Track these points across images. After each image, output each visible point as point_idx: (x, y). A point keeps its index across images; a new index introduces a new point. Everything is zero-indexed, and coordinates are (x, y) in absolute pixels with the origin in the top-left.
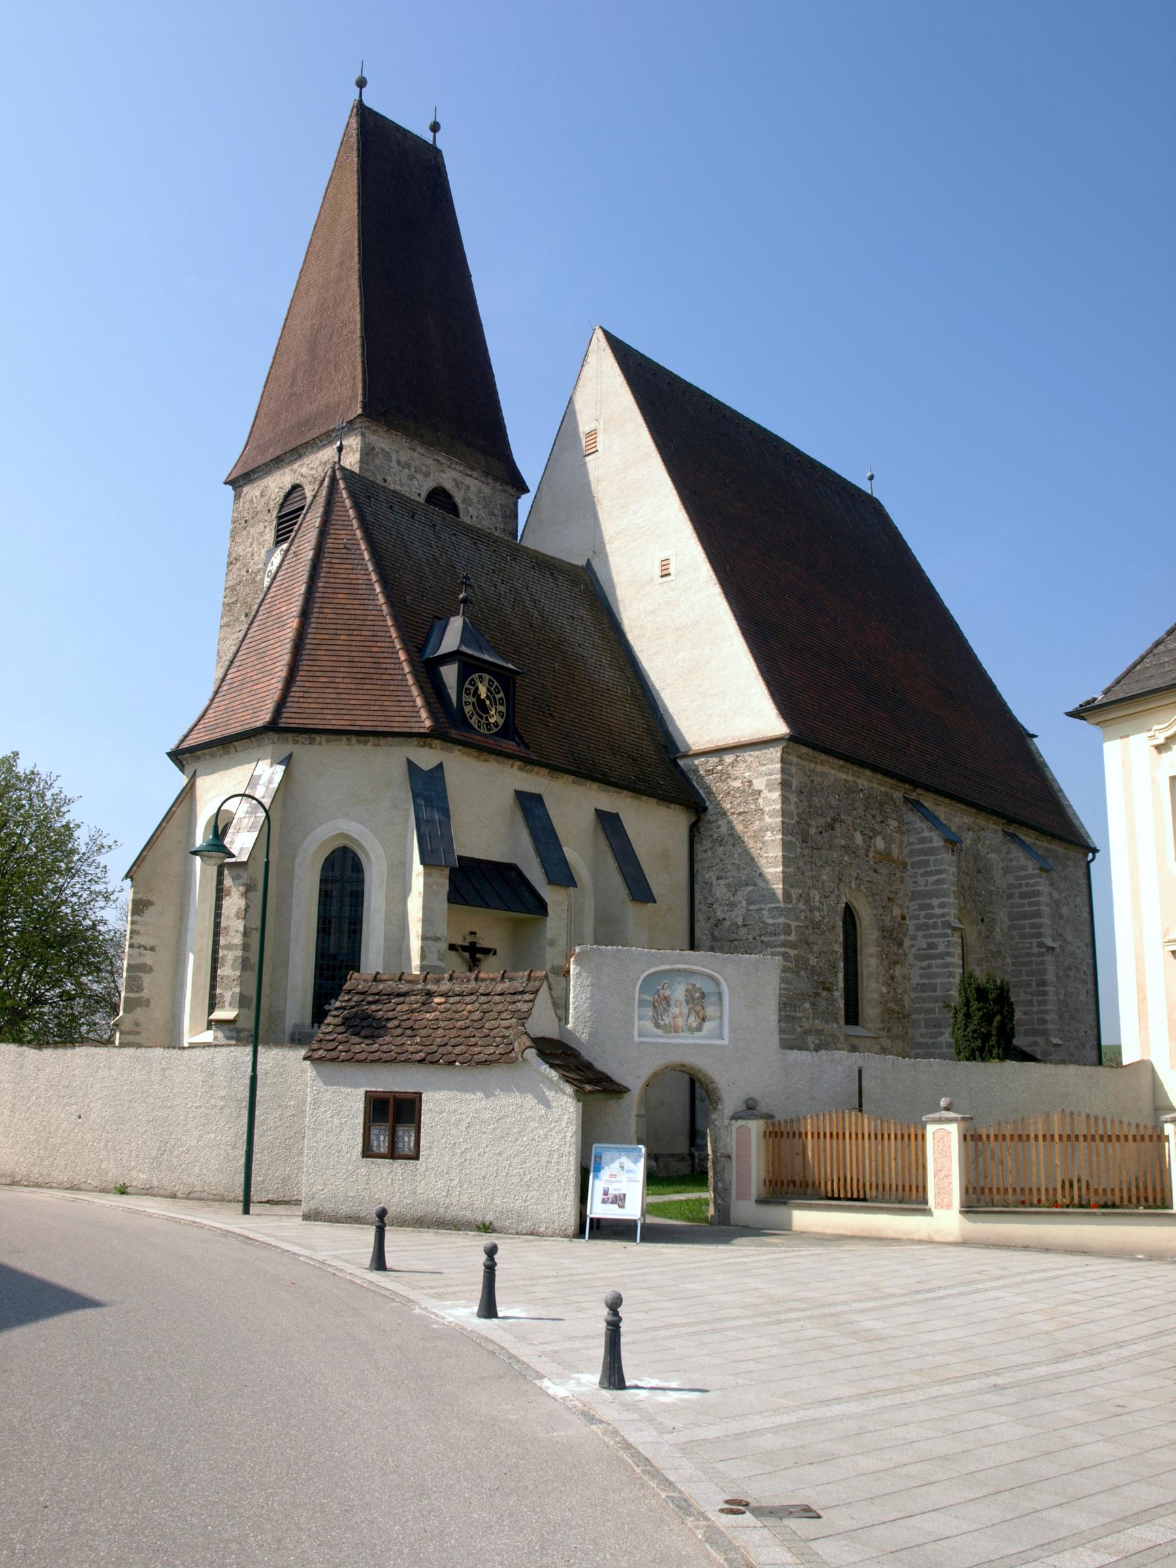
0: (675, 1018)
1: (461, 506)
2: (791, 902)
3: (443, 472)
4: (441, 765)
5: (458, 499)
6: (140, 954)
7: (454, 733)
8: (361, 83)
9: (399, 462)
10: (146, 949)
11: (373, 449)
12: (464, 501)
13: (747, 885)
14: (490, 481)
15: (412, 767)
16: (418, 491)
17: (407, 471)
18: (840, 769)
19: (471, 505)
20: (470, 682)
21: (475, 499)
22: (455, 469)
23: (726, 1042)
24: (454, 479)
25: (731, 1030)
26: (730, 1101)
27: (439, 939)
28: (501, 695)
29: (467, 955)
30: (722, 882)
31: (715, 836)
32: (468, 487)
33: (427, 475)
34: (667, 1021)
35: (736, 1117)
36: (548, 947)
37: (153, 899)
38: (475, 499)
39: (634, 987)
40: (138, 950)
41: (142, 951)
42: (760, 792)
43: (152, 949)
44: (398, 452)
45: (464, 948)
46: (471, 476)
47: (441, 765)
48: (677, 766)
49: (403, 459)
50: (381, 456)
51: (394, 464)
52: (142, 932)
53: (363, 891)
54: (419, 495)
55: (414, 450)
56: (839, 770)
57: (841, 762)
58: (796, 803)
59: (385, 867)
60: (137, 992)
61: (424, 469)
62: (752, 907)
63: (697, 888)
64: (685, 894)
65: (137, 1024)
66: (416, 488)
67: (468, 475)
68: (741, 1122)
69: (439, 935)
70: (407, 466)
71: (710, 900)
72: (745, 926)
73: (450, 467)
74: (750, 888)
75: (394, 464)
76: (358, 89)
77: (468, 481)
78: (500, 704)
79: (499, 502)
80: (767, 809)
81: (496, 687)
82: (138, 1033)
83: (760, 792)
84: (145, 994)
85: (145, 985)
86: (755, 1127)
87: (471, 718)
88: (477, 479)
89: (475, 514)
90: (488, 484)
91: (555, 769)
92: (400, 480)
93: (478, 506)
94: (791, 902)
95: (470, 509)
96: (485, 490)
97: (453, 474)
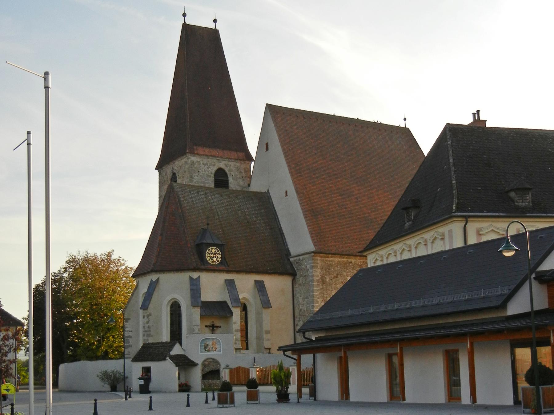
0: (209, 348)
1: (228, 173)
2: (318, 303)
3: (220, 162)
4: (199, 277)
5: (227, 171)
6: (128, 333)
7: (203, 267)
8: (184, 15)
9: (203, 164)
10: (130, 331)
11: (193, 162)
12: (229, 170)
13: (307, 298)
14: (239, 161)
15: (191, 278)
16: (211, 172)
17: (207, 166)
18: (340, 258)
19: (232, 171)
20: (208, 250)
21: (233, 169)
22: (225, 161)
23: (221, 353)
24: (225, 164)
25: (222, 350)
26: (223, 366)
27: (198, 325)
28: (220, 252)
29: (211, 328)
30: (301, 297)
31: (299, 283)
32: (231, 165)
33: (214, 165)
34: (208, 349)
35: (224, 369)
36: (234, 325)
37: (130, 318)
38: (233, 169)
39: (199, 342)
40: (128, 332)
41: (129, 332)
42: (309, 269)
43: (131, 331)
44: (202, 160)
45: (210, 326)
46: (231, 161)
47: (199, 277)
48: (290, 260)
49: (205, 162)
50: (196, 163)
51: (202, 165)
52: (128, 327)
53: (181, 313)
54: (212, 173)
55: (209, 158)
56: (339, 258)
57: (339, 256)
58: (320, 272)
59: (186, 306)
60: (128, 343)
61: (213, 164)
62: (308, 305)
63: (295, 300)
64: (291, 301)
65: (129, 352)
66: (210, 171)
67: (230, 161)
68: (225, 370)
69: (198, 324)
70: (207, 164)
71: (299, 303)
72: (307, 311)
73: (223, 160)
74: (307, 299)
75: (202, 165)
76: (184, 18)
77: (230, 163)
78: (219, 255)
79: (243, 167)
80: (310, 275)
81: (218, 250)
82: (130, 354)
83: (309, 269)
84: (131, 344)
85: (130, 341)
86: (227, 371)
87: (209, 261)
88: (234, 161)
89: (234, 174)
90: (238, 162)
91: (238, 272)
92: (204, 170)
93: (235, 171)
94: (318, 303)
95: (232, 173)
96: (237, 165)
97: (224, 162)
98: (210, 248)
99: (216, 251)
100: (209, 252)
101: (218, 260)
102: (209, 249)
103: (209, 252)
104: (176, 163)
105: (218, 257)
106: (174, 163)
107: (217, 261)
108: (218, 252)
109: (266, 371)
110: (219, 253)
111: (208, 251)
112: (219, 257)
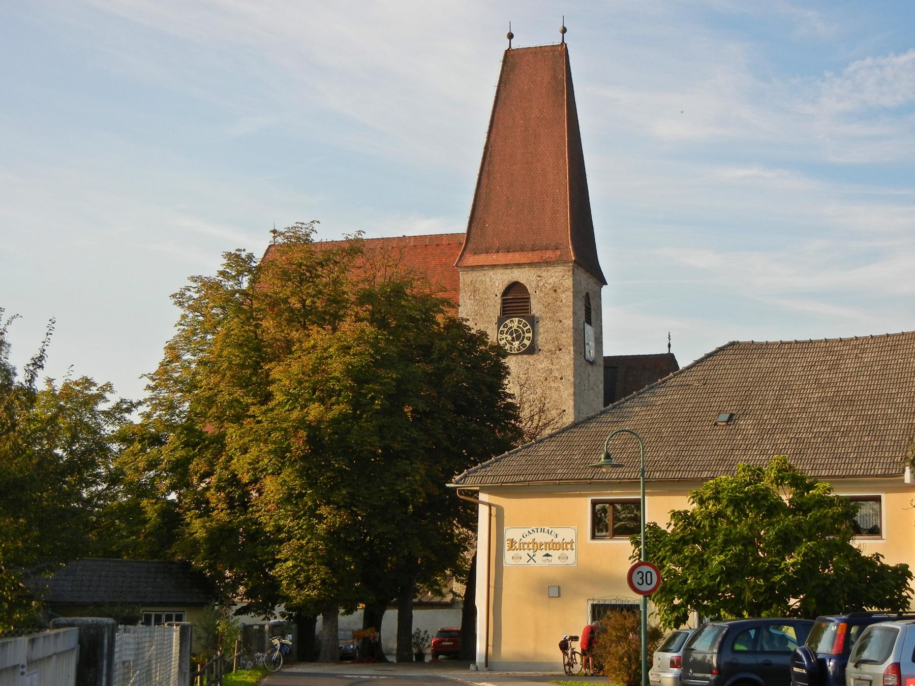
28: (529, 327)
98: (509, 321)
99: (521, 326)
100: (506, 329)
101: (524, 344)
102: (506, 324)
103: (506, 329)
104: (590, 280)
105: (524, 337)
106: (590, 278)
107: (522, 346)
108: (525, 327)
109: (786, 534)
110: (526, 330)
111: (504, 327)
112: (527, 338)
